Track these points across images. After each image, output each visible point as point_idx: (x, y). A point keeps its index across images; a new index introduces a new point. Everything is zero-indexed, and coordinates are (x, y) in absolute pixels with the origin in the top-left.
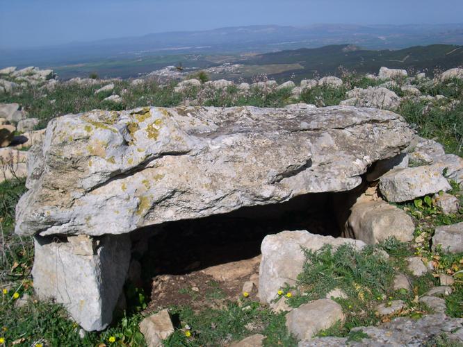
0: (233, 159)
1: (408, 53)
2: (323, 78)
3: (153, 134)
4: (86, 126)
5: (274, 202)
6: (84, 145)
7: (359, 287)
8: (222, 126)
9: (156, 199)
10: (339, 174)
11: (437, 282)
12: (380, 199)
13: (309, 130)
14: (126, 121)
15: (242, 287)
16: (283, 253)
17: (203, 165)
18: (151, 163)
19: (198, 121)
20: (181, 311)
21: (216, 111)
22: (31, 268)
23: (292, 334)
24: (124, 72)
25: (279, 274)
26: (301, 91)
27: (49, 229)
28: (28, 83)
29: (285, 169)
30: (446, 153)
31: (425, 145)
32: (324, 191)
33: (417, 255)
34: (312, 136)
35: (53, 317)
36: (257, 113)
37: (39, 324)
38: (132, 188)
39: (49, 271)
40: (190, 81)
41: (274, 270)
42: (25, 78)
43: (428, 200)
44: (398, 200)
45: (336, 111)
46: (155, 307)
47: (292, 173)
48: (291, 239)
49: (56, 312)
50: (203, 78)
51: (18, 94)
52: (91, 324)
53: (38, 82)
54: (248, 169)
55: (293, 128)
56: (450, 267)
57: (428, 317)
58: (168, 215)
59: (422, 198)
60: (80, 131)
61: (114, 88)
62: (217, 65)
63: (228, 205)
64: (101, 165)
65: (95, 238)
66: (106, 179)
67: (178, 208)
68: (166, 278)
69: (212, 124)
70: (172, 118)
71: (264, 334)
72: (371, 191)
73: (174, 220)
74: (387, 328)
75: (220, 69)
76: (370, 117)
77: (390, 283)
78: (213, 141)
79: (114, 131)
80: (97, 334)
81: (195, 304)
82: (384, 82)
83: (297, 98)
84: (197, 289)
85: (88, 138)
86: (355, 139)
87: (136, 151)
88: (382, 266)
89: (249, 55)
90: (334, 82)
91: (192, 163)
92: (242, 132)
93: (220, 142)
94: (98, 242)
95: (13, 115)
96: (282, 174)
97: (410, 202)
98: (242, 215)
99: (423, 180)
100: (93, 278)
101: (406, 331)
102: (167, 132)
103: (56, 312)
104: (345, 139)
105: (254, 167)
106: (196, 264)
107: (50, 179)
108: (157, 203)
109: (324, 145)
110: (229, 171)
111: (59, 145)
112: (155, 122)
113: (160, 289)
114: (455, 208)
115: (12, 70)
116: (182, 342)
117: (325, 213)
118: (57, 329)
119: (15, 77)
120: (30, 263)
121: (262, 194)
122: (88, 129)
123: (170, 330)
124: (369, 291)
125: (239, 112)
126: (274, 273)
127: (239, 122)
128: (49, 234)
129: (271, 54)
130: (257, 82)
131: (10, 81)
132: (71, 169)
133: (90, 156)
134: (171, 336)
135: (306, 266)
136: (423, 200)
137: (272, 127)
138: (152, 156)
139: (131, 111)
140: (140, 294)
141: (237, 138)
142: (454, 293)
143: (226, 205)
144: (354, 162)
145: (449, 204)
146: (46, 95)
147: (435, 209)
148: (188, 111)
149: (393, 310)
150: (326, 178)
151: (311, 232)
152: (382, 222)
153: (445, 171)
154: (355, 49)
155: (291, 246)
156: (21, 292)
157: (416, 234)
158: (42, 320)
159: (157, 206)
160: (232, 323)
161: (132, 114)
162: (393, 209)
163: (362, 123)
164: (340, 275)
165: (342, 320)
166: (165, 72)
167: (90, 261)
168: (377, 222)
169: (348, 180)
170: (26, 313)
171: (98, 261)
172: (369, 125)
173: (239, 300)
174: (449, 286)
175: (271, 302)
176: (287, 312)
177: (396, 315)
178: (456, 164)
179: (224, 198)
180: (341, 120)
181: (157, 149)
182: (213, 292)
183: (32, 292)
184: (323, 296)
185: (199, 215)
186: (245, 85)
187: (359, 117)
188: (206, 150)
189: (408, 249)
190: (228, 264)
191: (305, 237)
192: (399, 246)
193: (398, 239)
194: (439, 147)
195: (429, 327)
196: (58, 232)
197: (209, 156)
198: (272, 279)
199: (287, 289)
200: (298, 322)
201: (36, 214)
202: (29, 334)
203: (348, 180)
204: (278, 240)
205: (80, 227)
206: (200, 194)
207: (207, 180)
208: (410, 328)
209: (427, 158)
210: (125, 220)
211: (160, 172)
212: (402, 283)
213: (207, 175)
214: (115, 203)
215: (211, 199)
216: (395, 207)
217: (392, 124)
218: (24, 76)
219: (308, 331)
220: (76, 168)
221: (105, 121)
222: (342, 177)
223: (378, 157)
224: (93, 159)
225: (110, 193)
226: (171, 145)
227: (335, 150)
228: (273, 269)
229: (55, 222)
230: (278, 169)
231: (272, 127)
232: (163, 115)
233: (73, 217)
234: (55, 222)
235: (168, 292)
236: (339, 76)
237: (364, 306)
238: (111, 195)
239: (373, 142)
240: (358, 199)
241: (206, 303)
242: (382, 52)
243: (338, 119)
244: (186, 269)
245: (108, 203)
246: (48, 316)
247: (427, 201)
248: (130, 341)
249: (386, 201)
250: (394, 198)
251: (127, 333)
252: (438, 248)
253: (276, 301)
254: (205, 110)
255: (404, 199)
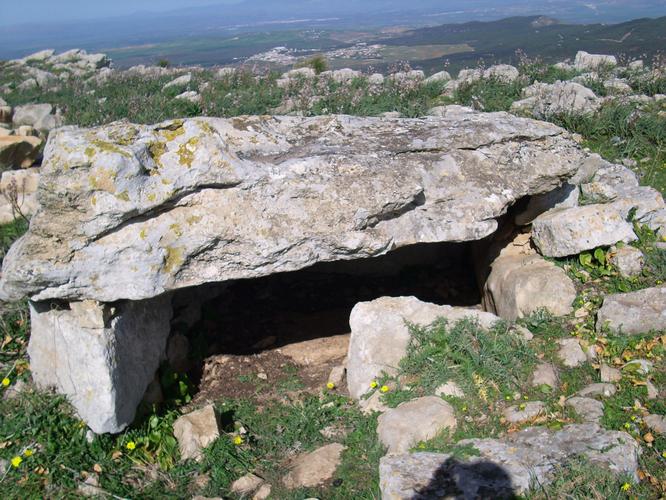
0: (305, 194)
1: (628, 30)
2: (489, 69)
3: (186, 158)
4: (88, 149)
5: (365, 256)
6: (84, 175)
7: (481, 381)
8: (297, 144)
9: (190, 250)
10: (464, 216)
11: (596, 376)
12: (533, 251)
13: (424, 151)
14: (147, 140)
15: (328, 374)
16: (379, 329)
17: (264, 202)
18: (184, 200)
19: (262, 138)
20: (237, 406)
21: (292, 122)
22: (27, 345)
23: (382, 445)
24: (208, 56)
25: (373, 357)
26: (457, 86)
27: (42, 292)
28: (71, 73)
29: (380, 208)
30: (640, 185)
31: (610, 173)
32: (441, 240)
33: (575, 336)
34: (427, 159)
35: (51, 413)
36: (352, 125)
37: (32, 422)
38: (156, 235)
39: (49, 349)
40: (300, 70)
41: (367, 352)
42: (66, 66)
43: (599, 255)
44: (556, 254)
45: (467, 123)
46: (204, 401)
47: (393, 213)
48: (391, 309)
49: (56, 406)
50: (319, 67)
51: (55, 89)
52: (101, 424)
53: (84, 72)
54: (325, 207)
55: (400, 149)
56: (619, 355)
57: (572, 428)
58: (210, 273)
59: (591, 252)
60: (78, 156)
61: (191, 82)
62: (348, 46)
63: (296, 260)
64: (107, 204)
65: (108, 305)
66: (117, 224)
67: (224, 264)
68: (224, 359)
69: (282, 142)
70: (215, 134)
71: (344, 443)
72: (522, 239)
73: (219, 280)
74: (512, 441)
75: (352, 51)
76: (517, 132)
77: (528, 376)
78: (277, 168)
79: (127, 155)
80: (113, 437)
81: (260, 398)
82: (579, 74)
83: (451, 97)
84: (265, 377)
85: (89, 165)
86: (491, 164)
87: (160, 183)
88: (521, 352)
89: (394, 31)
90: (507, 73)
91: (245, 199)
92: (323, 154)
93: (287, 169)
94: (113, 310)
95: (43, 121)
96: (377, 216)
97: (574, 258)
98: (317, 273)
99: (593, 226)
100: (101, 361)
101: (539, 447)
102: (206, 155)
103: (56, 406)
104: (476, 163)
105: (334, 206)
106: (270, 340)
107: (41, 223)
108: (192, 256)
109: (444, 172)
110: (297, 211)
111: (51, 175)
112: (189, 142)
113: (213, 374)
114: (638, 267)
115: (49, 55)
116: (230, 452)
117: (452, 273)
118: (56, 430)
119: (52, 65)
120: (27, 337)
121: (344, 244)
122: (90, 152)
123: (213, 434)
124: (496, 386)
125: (325, 124)
126: (366, 357)
127: (322, 139)
128: (43, 298)
129: (426, 29)
130: (395, 73)
131: (45, 70)
132: (69, 209)
133: (93, 191)
134: (215, 442)
135: (411, 348)
136: (593, 256)
137: (370, 146)
138: (184, 190)
139: (156, 126)
140: (181, 383)
141: (312, 162)
142: (619, 393)
143: (293, 260)
144: (487, 199)
145: (630, 261)
146: (93, 92)
147: (610, 268)
148: (249, 123)
149: (526, 416)
150: (445, 221)
151: (420, 299)
152: (529, 286)
153: (633, 211)
154: (549, 23)
155: (390, 318)
156: (13, 378)
157: (576, 305)
158: (35, 418)
159: (192, 260)
160: (302, 426)
161: (157, 130)
162: (547, 268)
163: (503, 142)
164: (455, 363)
165: (451, 427)
166: (272, 56)
167: (99, 336)
168: (522, 286)
169: (477, 225)
170: (17, 407)
171: (112, 337)
172: (515, 144)
173: (321, 394)
174: (614, 383)
175: (361, 397)
176: (379, 413)
177: (528, 423)
178: (652, 204)
179: (289, 249)
180: (472, 136)
181: (191, 180)
182: (287, 381)
183: (28, 378)
184: (430, 391)
185: (255, 273)
186: (378, 77)
187: (499, 132)
188: (264, 181)
189: (563, 326)
190: (315, 341)
191: (411, 306)
192: (551, 321)
193: (550, 311)
194: (630, 176)
195: (571, 442)
196: (55, 296)
197: (269, 190)
198: (363, 365)
199: (384, 379)
200: (390, 428)
201: (22, 271)
202: (19, 435)
203: (477, 225)
204: (373, 309)
205: (84, 290)
206: (254, 244)
207: (265, 224)
208: (543, 443)
209: (608, 191)
210: (147, 280)
211: (195, 212)
212: (545, 377)
213: (265, 216)
214: (132, 256)
215: (271, 251)
216: (552, 264)
217: (550, 142)
218: (65, 63)
219: (403, 442)
220: (75, 207)
221: (118, 140)
222: (468, 221)
223: (525, 191)
224: (97, 195)
225: (123, 242)
226: (212, 174)
227: (461, 181)
228: (365, 352)
229: (49, 283)
230: (369, 209)
231: (370, 146)
232: (201, 131)
233: (73, 275)
234: (49, 283)
235: (224, 379)
236: (515, 64)
237: (486, 408)
238: (125, 245)
239: (519, 168)
240: (504, 252)
241: (274, 396)
242: (591, 27)
243: (467, 134)
244: (255, 346)
245: (122, 256)
246: (44, 412)
247: (598, 257)
248: (157, 449)
249: (542, 255)
250: (551, 252)
251: (153, 437)
252: (604, 326)
253: (367, 396)
254: (277, 120)
255: (565, 253)
